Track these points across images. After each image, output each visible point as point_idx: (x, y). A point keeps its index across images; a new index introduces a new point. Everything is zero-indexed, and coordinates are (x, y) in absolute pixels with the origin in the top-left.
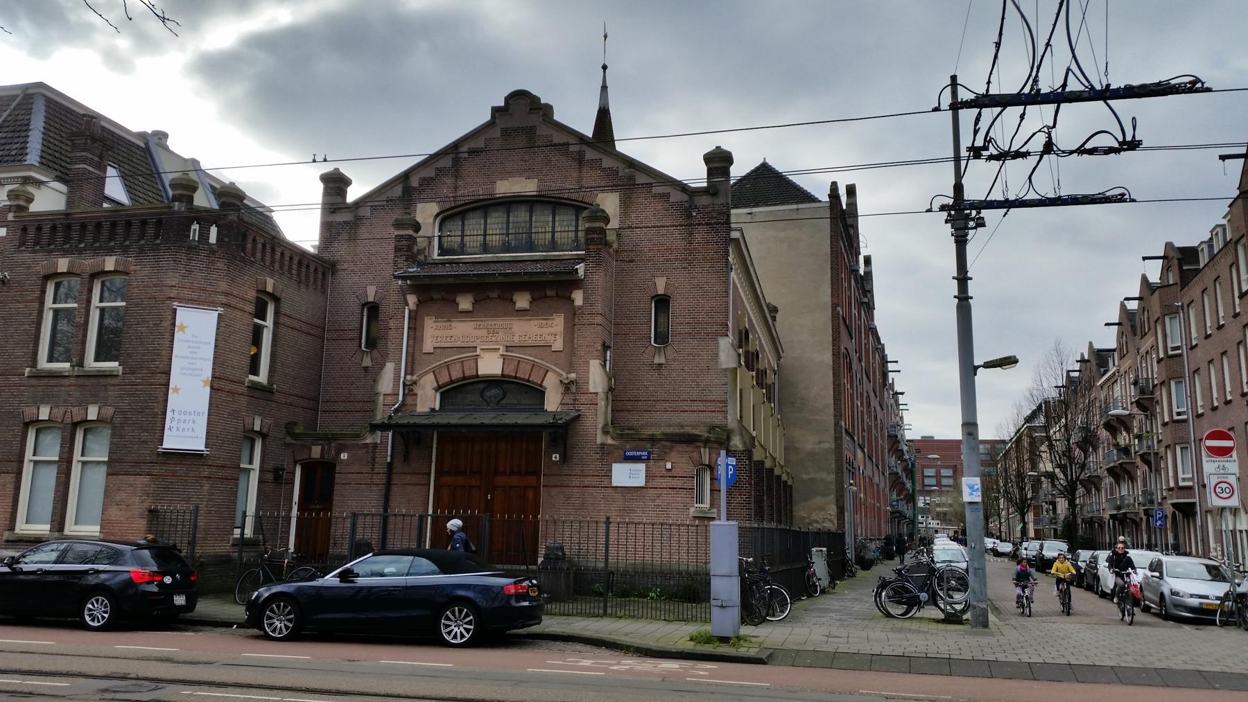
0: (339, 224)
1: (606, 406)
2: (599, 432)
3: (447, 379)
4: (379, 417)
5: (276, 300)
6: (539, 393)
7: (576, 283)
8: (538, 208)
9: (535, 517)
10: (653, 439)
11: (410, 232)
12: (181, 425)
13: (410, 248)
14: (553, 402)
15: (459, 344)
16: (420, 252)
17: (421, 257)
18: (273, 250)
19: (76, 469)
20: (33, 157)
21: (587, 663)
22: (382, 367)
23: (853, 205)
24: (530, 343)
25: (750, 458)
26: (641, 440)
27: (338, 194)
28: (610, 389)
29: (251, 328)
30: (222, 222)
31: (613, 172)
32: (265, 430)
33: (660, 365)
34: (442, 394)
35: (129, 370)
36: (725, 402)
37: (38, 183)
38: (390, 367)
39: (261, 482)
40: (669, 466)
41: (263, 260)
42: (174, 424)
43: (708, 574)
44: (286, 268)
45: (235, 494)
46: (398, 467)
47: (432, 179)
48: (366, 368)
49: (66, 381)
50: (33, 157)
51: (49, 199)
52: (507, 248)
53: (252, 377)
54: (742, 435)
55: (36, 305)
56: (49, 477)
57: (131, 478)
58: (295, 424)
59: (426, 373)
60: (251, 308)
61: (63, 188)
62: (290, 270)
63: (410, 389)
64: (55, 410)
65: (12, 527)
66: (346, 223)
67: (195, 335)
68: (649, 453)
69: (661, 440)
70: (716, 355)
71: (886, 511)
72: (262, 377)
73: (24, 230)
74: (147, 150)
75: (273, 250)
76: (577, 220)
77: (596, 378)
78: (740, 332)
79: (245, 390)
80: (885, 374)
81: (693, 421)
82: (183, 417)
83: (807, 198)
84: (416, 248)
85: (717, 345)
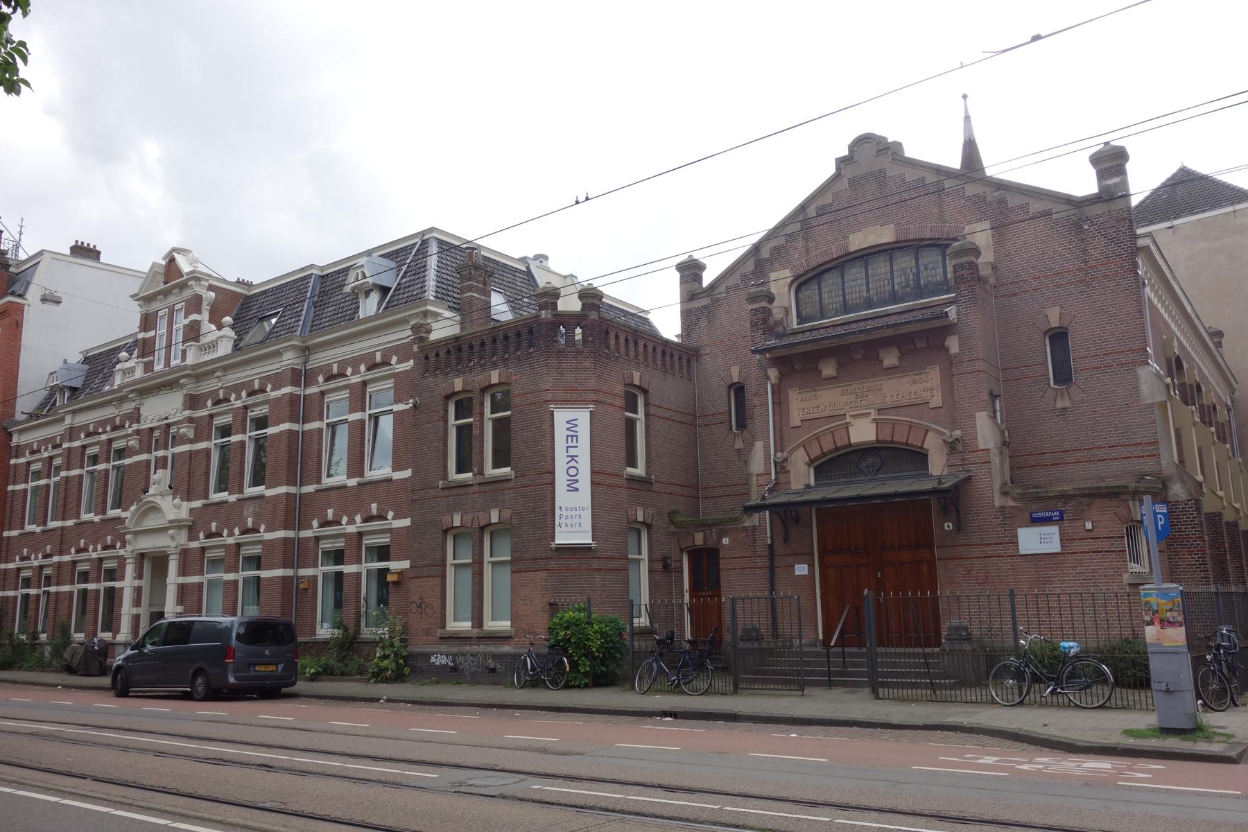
0: (698, 309)
1: (1002, 464)
2: (997, 495)
3: (818, 452)
4: (755, 500)
5: (645, 392)
6: (919, 458)
7: (948, 329)
8: (898, 254)
9: (934, 592)
10: (1064, 497)
11: (764, 304)
12: (569, 521)
13: (765, 320)
14: (938, 464)
15: (827, 413)
17: (780, 329)
18: (636, 343)
19: (487, 570)
20: (430, 294)
21: (989, 760)
22: (751, 446)
24: (904, 402)
25: (1198, 509)
26: (1050, 498)
27: (695, 280)
28: (1005, 443)
29: (623, 422)
30: (584, 323)
31: (981, 199)
32: (648, 521)
34: (816, 469)
35: (520, 474)
36: (1156, 443)
38: (759, 445)
39: (651, 571)
40: (1089, 526)
41: (627, 354)
42: (563, 521)
43: (1146, 653)
44: (650, 360)
45: (627, 584)
46: (780, 548)
47: (782, 247)
48: (738, 450)
49: (470, 490)
51: (445, 326)
52: (846, 308)
53: (630, 470)
54: (1183, 482)
55: (442, 423)
56: (467, 576)
57: (532, 574)
60: (621, 402)
62: (654, 362)
63: (781, 467)
65: (443, 625)
66: (705, 307)
67: (572, 434)
68: (1061, 512)
69: (1074, 496)
72: (640, 470)
73: (427, 358)
74: (529, 273)
75: (636, 343)
76: (944, 261)
77: (985, 432)
78: (1169, 361)
81: (1110, 473)
82: (569, 513)
84: (771, 322)
85: (1136, 377)
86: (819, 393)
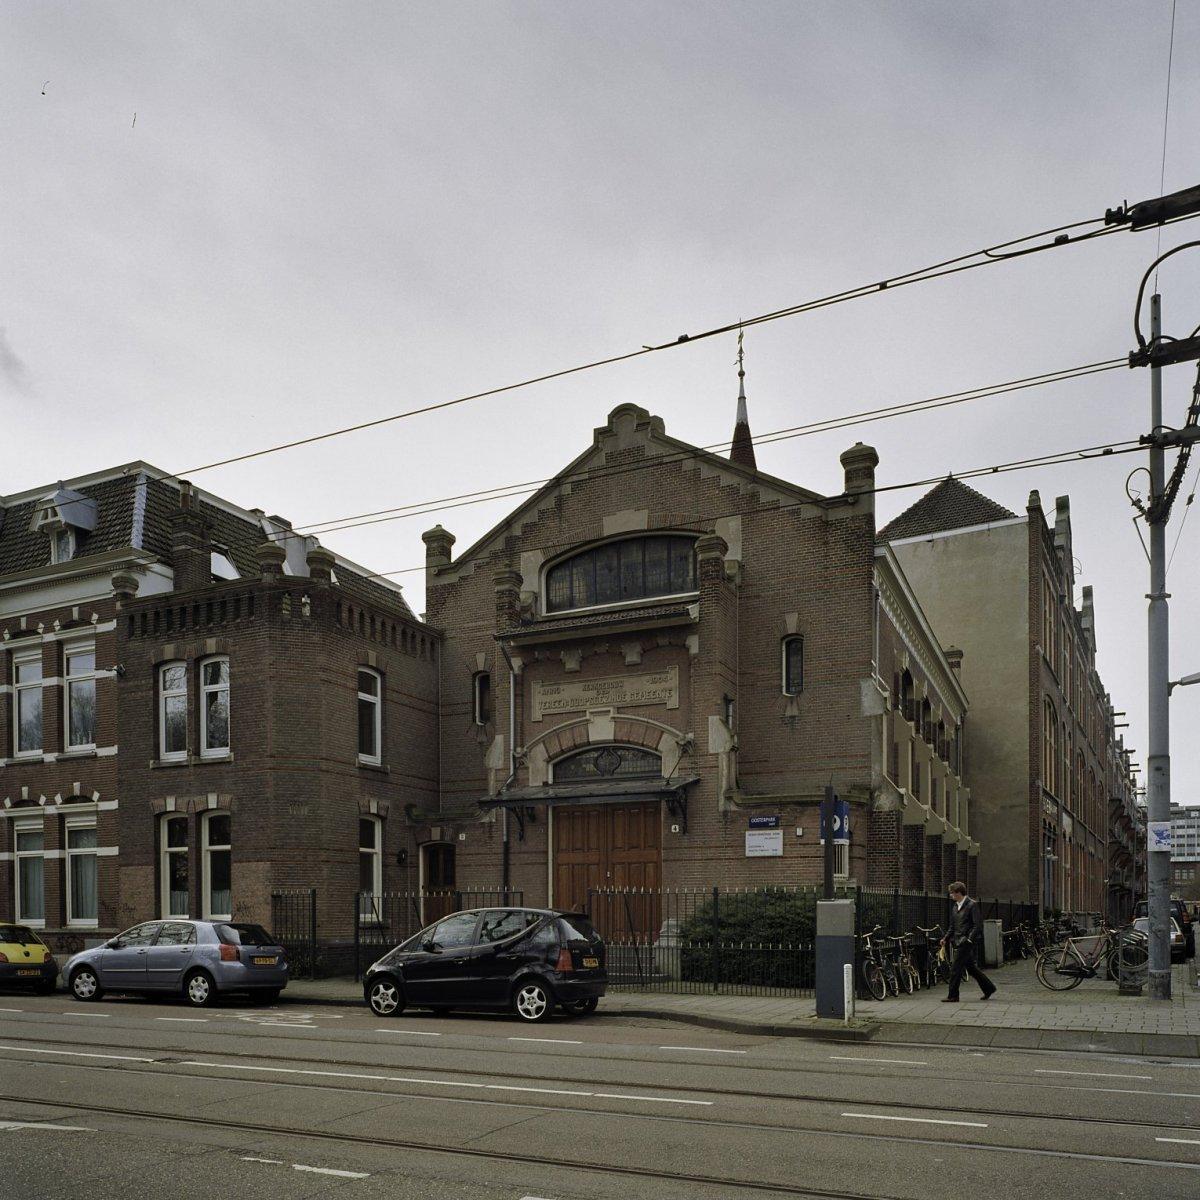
2: (722, 798)
7: (689, 628)
10: (782, 804)
13: (511, 606)
16: (525, 609)
17: (528, 616)
18: (373, 620)
20: (136, 539)
23: (1065, 524)
24: (643, 701)
29: (356, 706)
32: (383, 813)
33: (793, 717)
37: (143, 569)
38: (499, 739)
40: (799, 832)
44: (388, 639)
46: (515, 845)
47: (535, 524)
50: (136, 539)
51: (155, 582)
57: (253, 865)
58: (415, 806)
59: (535, 744)
61: (169, 572)
62: (394, 642)
63: (520, 763)
64: (179, 801)
68: (777, 819)
70: (859, 703)
71: (1104, 885)
72: (375, 760)
73: (132, 618)
75: (373, 620)
77: (717, 739)
79: (356, 772)
80: (1109, 729)
83: (995, 512)
86: (561, 687)
